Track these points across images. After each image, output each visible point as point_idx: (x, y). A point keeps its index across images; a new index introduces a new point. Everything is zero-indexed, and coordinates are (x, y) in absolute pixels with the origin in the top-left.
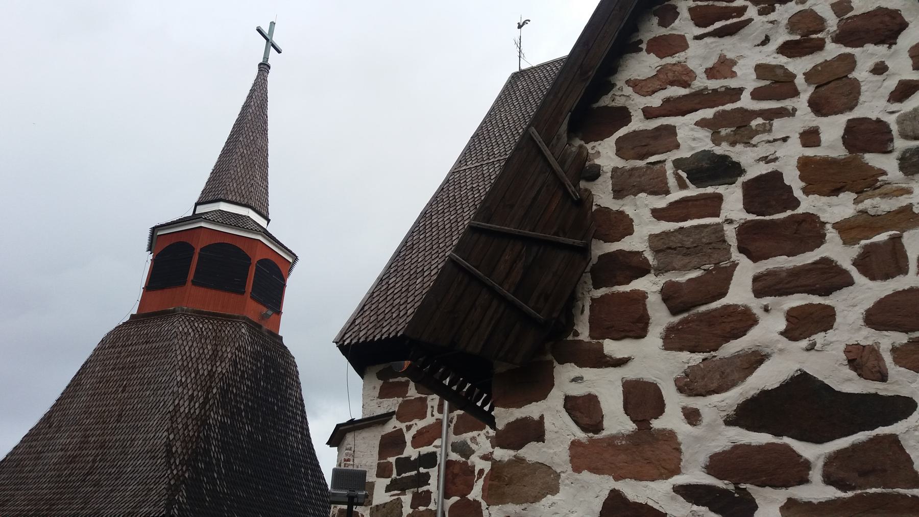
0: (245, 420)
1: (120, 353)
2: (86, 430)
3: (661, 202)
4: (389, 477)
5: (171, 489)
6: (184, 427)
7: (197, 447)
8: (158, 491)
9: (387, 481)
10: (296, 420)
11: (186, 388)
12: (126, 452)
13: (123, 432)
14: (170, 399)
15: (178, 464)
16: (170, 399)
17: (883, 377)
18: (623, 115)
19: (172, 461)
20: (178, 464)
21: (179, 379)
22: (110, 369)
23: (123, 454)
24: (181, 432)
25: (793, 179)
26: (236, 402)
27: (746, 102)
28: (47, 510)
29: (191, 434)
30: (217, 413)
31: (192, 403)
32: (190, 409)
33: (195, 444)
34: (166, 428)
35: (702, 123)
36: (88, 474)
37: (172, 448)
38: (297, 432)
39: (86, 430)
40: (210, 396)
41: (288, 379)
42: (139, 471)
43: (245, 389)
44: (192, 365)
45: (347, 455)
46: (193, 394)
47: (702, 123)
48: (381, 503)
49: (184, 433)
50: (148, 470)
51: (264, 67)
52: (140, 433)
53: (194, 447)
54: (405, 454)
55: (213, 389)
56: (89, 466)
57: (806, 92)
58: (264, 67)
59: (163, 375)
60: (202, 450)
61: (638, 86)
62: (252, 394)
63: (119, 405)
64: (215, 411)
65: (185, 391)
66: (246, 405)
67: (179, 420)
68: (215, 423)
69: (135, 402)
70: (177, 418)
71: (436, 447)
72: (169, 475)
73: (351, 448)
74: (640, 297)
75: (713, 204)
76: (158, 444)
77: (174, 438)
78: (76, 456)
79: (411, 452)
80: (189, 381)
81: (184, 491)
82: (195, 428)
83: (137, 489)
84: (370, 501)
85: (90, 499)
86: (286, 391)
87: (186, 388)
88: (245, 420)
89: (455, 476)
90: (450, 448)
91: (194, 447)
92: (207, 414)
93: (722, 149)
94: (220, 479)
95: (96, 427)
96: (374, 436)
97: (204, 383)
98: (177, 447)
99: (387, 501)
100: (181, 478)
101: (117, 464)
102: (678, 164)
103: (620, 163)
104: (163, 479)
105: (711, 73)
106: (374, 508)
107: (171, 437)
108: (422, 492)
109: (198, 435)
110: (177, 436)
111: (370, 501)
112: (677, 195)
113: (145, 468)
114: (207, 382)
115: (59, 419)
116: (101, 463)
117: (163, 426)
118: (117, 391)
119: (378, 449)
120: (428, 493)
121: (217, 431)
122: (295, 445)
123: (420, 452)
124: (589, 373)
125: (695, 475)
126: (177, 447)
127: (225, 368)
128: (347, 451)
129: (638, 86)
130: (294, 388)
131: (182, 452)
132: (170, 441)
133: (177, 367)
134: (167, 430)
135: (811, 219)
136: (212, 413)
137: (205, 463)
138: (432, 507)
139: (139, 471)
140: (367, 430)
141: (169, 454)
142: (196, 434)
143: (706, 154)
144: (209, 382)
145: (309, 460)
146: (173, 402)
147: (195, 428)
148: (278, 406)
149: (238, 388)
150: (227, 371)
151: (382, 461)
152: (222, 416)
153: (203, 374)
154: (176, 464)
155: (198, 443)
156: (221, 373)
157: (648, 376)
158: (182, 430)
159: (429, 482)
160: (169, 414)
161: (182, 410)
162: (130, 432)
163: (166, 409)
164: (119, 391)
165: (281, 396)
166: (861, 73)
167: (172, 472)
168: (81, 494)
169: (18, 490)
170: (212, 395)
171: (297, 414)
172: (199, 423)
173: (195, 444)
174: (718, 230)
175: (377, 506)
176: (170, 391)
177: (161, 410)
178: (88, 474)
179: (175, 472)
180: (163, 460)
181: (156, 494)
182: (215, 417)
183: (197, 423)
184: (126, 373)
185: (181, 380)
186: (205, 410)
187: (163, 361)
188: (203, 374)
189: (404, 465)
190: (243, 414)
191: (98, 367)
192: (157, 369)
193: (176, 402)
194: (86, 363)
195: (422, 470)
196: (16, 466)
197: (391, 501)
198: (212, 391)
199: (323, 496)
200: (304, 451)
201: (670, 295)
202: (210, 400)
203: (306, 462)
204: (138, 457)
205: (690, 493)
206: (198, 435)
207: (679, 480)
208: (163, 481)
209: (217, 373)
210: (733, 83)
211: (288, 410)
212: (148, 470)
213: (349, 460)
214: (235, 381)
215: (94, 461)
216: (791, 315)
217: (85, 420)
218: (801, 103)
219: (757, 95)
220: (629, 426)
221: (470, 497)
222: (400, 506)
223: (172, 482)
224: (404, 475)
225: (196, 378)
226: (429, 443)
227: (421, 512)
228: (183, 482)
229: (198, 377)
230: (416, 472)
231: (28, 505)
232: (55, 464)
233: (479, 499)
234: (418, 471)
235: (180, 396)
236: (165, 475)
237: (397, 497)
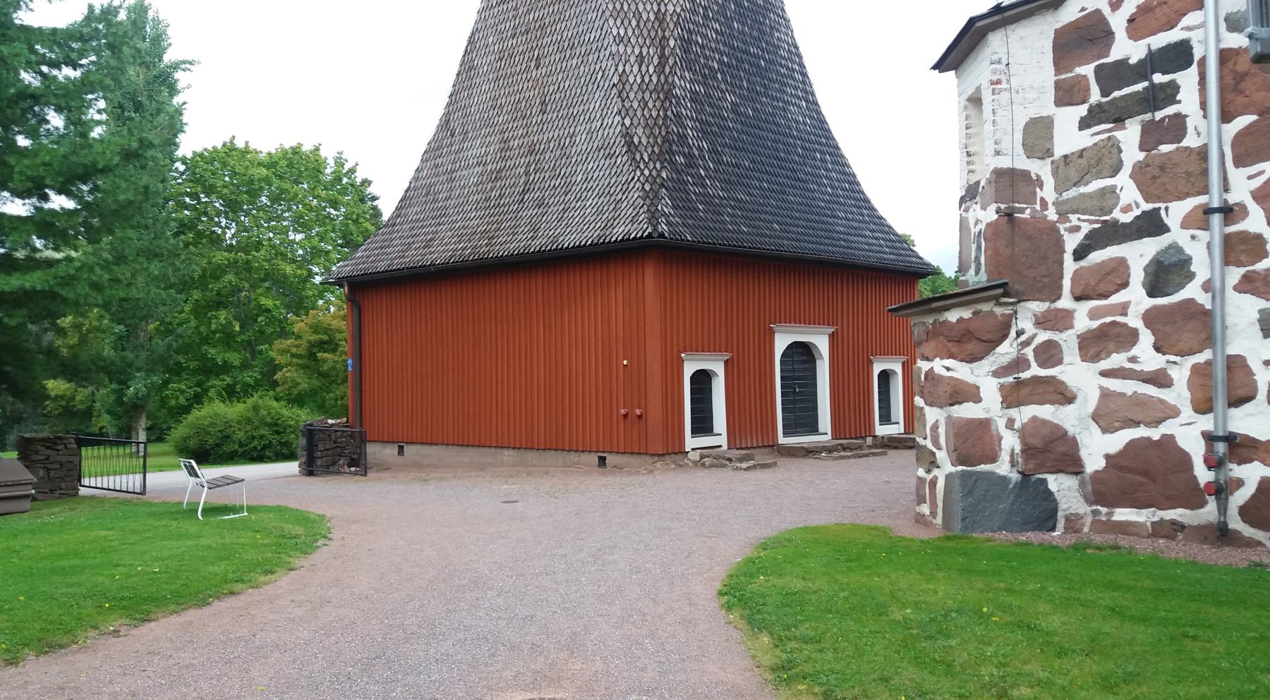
0: (723, 86)
1: (516, 9)
2: (503, 132)
4: (1084, 102)
5: (648, 197)
6: (641, 104)
7: (668, 133)
8: (631, 202)
9: (1082, 110)
10: (794, 79)
11: (629, 45)
12: (567, 154)
13: (554, 127)
14: (609, 65)
15: (647, 160)
16: (609, 65)
19: (638, 157)
20: (647, 160)
21: (615, 32)
22: (509, 36)
23: (565, 158)
24: (639, 113)
26: (706, 57)
28: (487, 245)
29: (654, 114)
30: (682, 78)
31: (644, 68)
32: (643, 77)
33: (663, 128)
34: (616, 110)
36: (524, 192)
37: (632, 138)
38: (799, 98)
39: (503, 132)
40: (666, 53)
41: (772, 15)
42: (594, 178)
43: (714, 36)
44: (629, 7)
45: (994, 72)
46: (641, 52)
48: (1073, 151)
49: (643, 114)
50: (606, 176)
52: (579, 124)
53: (663, 133)
54: (1115, 54)
55: (668, 40)
56: (522, 180)
59: (590, 30)
60: (675, 137)
62: (725, 44)
63: (537, 89)
64: (679, 74)
65: (629, 50)
66: (720, 62)
67: (632, 95)
68: (683, 94)
69: (560, 79)
70: (628, 93)
71: (1189, 29)
72: (639, 177)
73: (1000, 59)
76: (611, 135)
77: (632, 124)
78: (500, 171)
79: (1127, 49)
80: (630, 32)
81: (667, 199)
82: (657, 104)
83: (599, 203)
84: (1049, 149)
85: (539, 225)
86: (772, 36)
87: (629, 45)
88: (723, 86)
89: (1241, 77)
90: (1223, 25)
91: (663, 133)
92: (670, 80)
94: (710, 177)
95: (515, 126)
96: (1041, 33)
97: (653, 34)
98: (640, 135)
99: (1085, 146)
100: (658, 180)
101: (560, 174)
104: (632, 184)
106: (1059, 159)
107: (627, 122)
108: (1163, 119)
109: (666, 115)
110: (636, 121)
111: (1049, 149)
113: (602, 173)
114: (657, 31)
115: (461, 122)
116: (538, 174)
117: (611, 107)
118: (529, 67)
119: (1051, 55)
121: (689, 105)
122: (801, 119)
123: (1149, 45)
126: (640, 135)
127: (678, 5)
128: (993, 66)
130: (783, 28)
131: (648, 142)
132: (627, 128)
133: (607, 13)
134: (619, 113)
136: (676, 78)
137: (685, 155)
138: (1190, 141)
139: (594, 178)
140: (1024, 22)
141: (631, 147)
142: (661, 113)
144: (659, 30)
145: (824, 141)
146: (616, 70)
147: (657, 104)
148: (765, 60)
149: (704, 36)
150: (683, 9)
151: (1063, 77)
152: (691, 81)
153: (648, 19)
154: (644, 160)
155: (667, 127)
156: (675, 14)
158: (639, 109)
159: (1178, 98)
160: (614, 88)
161: (631, 79)
162: (565, 125)
163: (607, 81)
164: (532, 67)
165: (767, 43)
167: (642, 174)
168: (525, 220)
169: (439, 224)
170: (670, 50)
171: (793, 70)
172: (661, 96)
173: (663, 128)
175: (1066, 157)
176: (607, 53)
177: (601, 84)
178: (524, 192)
179: (646, 172)
180: (625, 158)
181: (628, 206)
182: (682, 84)
183: (659, 97)
184: (533, 38)
185: (618, 33)
186: (665, 74)
187: (583, 8)
188: (648, 19)
189: (1113, 75)
190: (719, 75)
191: (492, 37)
192: (579, 23)
193: (620, 69)
194: (473, 34)
195: (1158, 78)
196: (427, 194)
197: (1095, 144)
198: (668, 44)
199: (853, 191)
200: (814, 127)
202: (668, 59)
203: (820, 144)
204: (587, 158)
206: (666, 115)
208: (634, 187)
209: (668, 14)
211: (781, 65)
212: (606, 176)
213: (999, 82)
214: (697, 24)
215: (527, 173)
217: (497, 119)
222: (1115, 151)
223: (647, 187)
224: (1117, 94)
225: (639, 27)
226: (1171, 26)
227: (1165, 154)
228: (662, 186)
229: (642, 25)
230: (1146, 84)
231: (460, 242)
232: (476, 185)
234: (1151, 81)
235: (623, 58)
236: (633, 178)
237: (1106, 135)
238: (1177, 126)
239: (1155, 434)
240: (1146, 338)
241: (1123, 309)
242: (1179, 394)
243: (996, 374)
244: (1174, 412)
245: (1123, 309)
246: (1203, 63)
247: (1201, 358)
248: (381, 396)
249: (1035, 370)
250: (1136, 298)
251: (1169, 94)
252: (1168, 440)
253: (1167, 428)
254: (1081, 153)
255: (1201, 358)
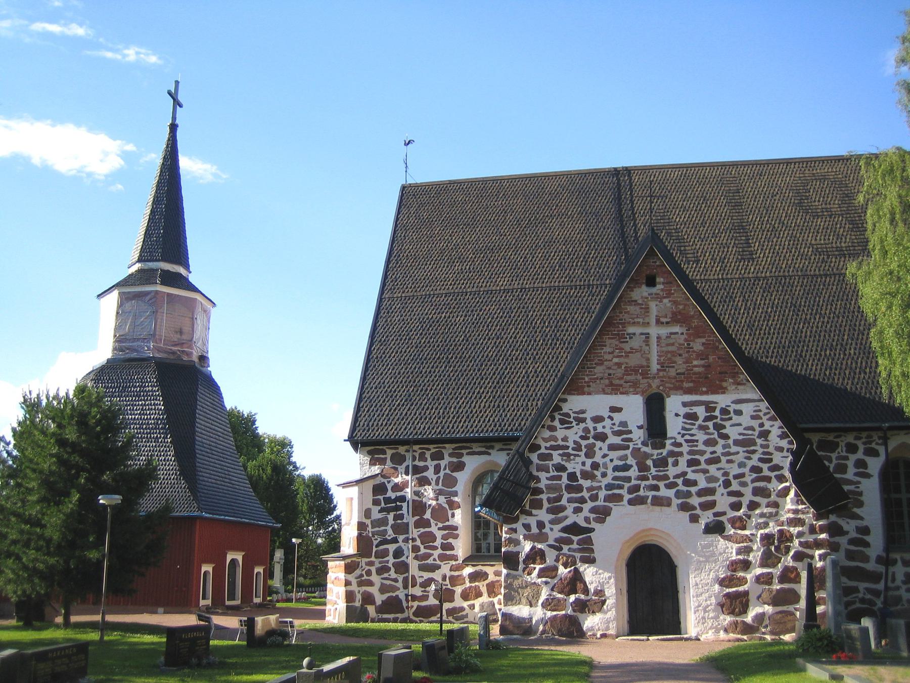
3: (548, 475)
17: (590, 524)
18: (539, 447)
25: (578, 474)
27: (570, 451)
35: (560, 455)
47: (560, 455)
51: (173, 127)
54: (388, 495)
57: (584, 450)
58: (173, 127)
61: (544, 439)
74: (541, 500)
75: (559, 478)
93: (563, 463)
102: (553, 465)
103: (538, 462)
105: (563, 440)
112: (552, 474)
120: (403, 515)
124: (528, 517)
125: (551, 542)
129: (544, 439)
135: (581, 485)
138: (405, 521)
143: (559, 463)
157: (542, 519)
166: (596, 449)
174: (560, 485)
189: (388, 500)
195: (398, 503)
201: (549, 500)
205: (550, 546)
207: (547, 543)
210: (568, 444)
216: (575, 508)
218: (582, 454)
219: (573, 449)
220: (538, 531)
221: (425, 517)
233: (429, 518)
238: (401, 517)
239: (394, 595)
240: (393, 570)
241: (388, 562)
242: (400, 584)
243: (356, 578)
244: (399, 589)
245: (388, 562)
246: (408, 502)
247: (405, 575)
248: (209, 416)
249: (365, 577)
250: (391, 559)
251: (400, 508)
252: (397, 596)
253: (397, 593)
254: (379, 519)
255: (405, 575)
